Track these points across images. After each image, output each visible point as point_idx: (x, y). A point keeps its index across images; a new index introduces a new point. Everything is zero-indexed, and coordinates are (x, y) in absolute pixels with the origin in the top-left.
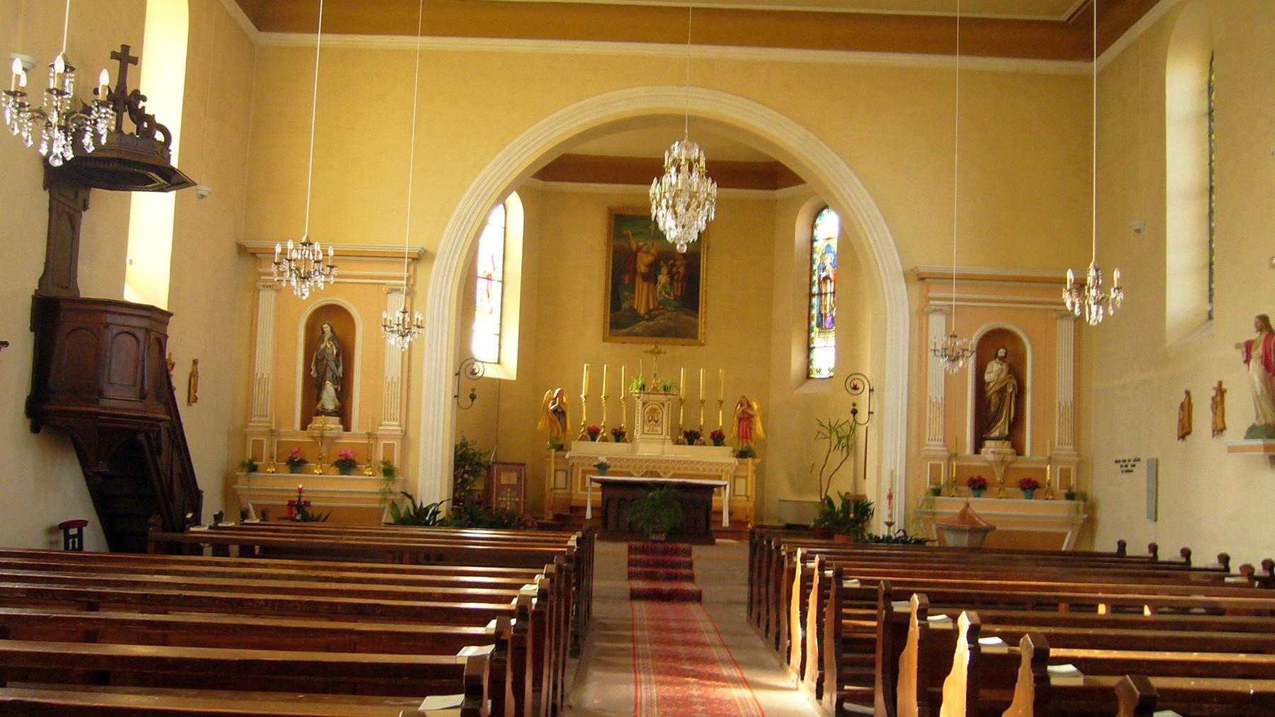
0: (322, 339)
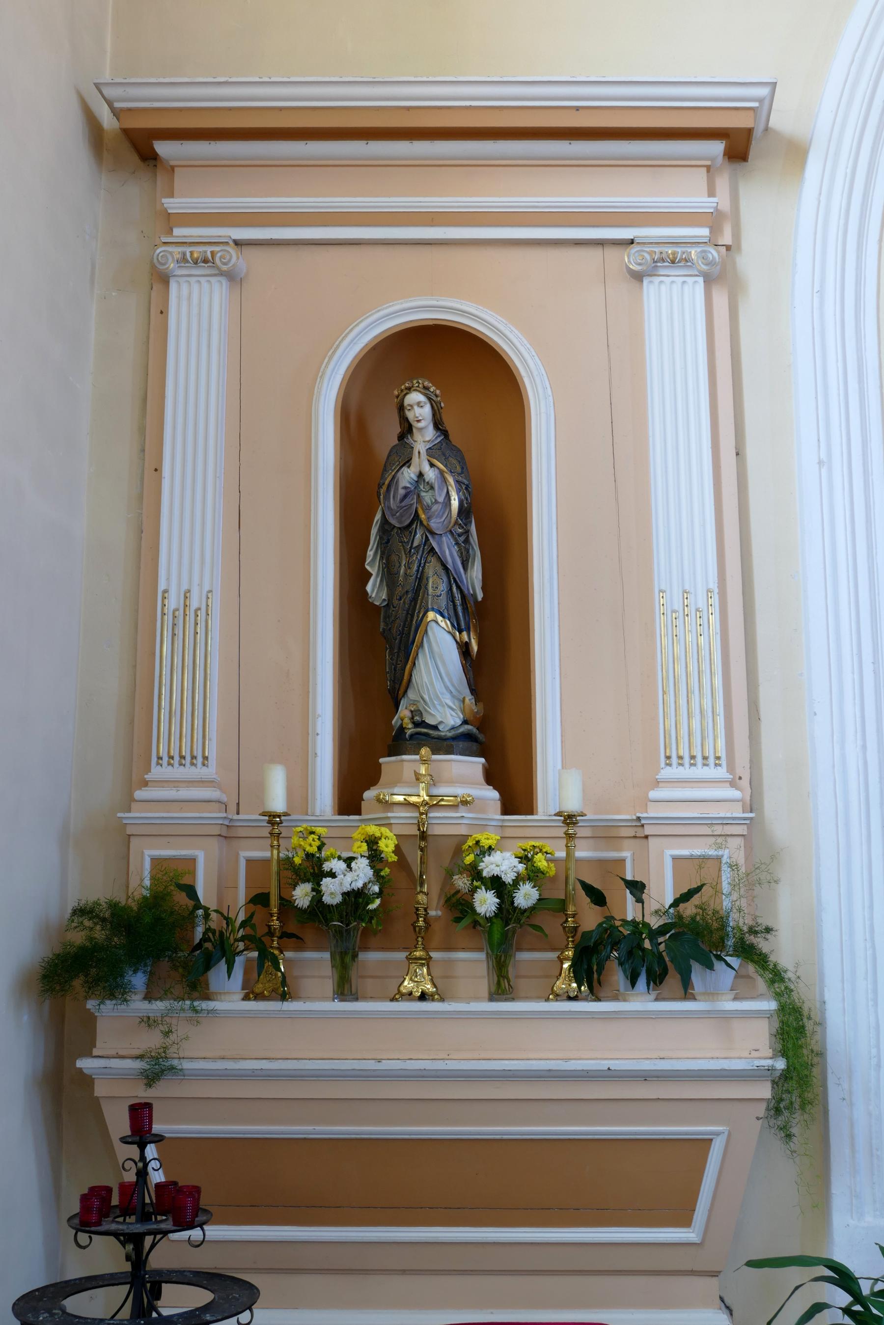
0: (402, 454)
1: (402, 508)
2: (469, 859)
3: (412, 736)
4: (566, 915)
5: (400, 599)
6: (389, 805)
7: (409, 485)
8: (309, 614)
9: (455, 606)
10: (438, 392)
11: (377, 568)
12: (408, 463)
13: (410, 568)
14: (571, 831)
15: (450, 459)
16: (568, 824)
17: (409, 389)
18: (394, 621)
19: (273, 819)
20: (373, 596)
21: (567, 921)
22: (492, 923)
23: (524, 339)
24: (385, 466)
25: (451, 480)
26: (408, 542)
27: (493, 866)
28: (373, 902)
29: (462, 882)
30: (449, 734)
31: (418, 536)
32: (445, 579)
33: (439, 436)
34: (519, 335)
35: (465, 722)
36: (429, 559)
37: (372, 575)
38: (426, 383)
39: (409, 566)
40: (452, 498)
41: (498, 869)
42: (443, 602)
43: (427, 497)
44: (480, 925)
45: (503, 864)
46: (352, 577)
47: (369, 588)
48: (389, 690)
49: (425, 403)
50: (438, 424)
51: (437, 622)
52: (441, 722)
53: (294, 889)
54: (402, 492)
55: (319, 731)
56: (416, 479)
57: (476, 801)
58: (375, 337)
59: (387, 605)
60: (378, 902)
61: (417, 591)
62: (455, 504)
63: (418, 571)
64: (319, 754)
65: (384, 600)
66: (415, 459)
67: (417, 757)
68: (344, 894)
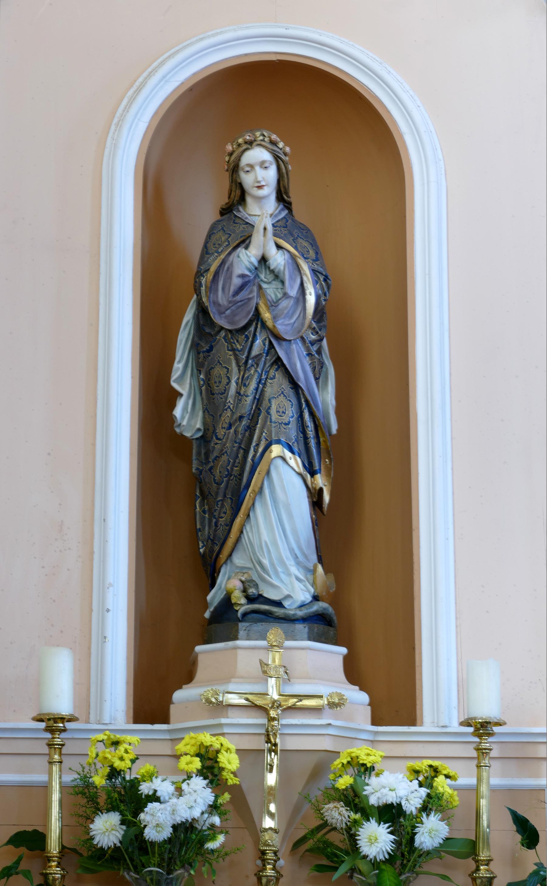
1: (236, 303)
2: (345, 781)
3: (245, 615)
4: (477, 861)
5: (230, 427)
6: (221, 708)
7: (247, 273)
8: (94, 445)
9: (306, 438)
10: (288, 149)
11: (187, 386)
12: (245, 242)
13: (245, 385)
14: (484, 746)
15: (300, 240)
16: (480, 736)
17: (250, 144)
18: (217, 458)
19: (54, 724)
20: (185, 423)
21: (478, 869)
22: (381, 871)
23: (405, 84)
24: (205, 246)
25: (305, 267)
26: (242, 350)
27: (385, 791)
28: (213, 838)
29: (338, 814)
30: (300, 613)
31: (258, 342)
32: (294, 401)
33: (282, 210)
34: (399, 78)
35: (316, 598)
36: (272, 373)
37: (181, 395)
38: (274, 137)
39: (243, 383)
40: (307, 292)
41: (393, 794)
42: (293, 431)
43: (271, 290)
44: (361, 873)
45: (392, 786)
46: (155, 398)
47: (178, 412)
48: (203, 556)
49: (271, 164)
50: (282, 196)
51: (283, 459)
52: (288, 597)
53: (93, 821)
54: (236, 282)
55: (110, 606)
56: (256, 264)
57: (347, 705)
58: (195, 74)
59: (202, 437)
60: (221, 838)
61: (254, 417)
62: (311, 300)
63: (257, 389)
64: (109, 638)
65: (199, 430)
66: (257, 238)
67: (263, 643)
68: (174, 827)
